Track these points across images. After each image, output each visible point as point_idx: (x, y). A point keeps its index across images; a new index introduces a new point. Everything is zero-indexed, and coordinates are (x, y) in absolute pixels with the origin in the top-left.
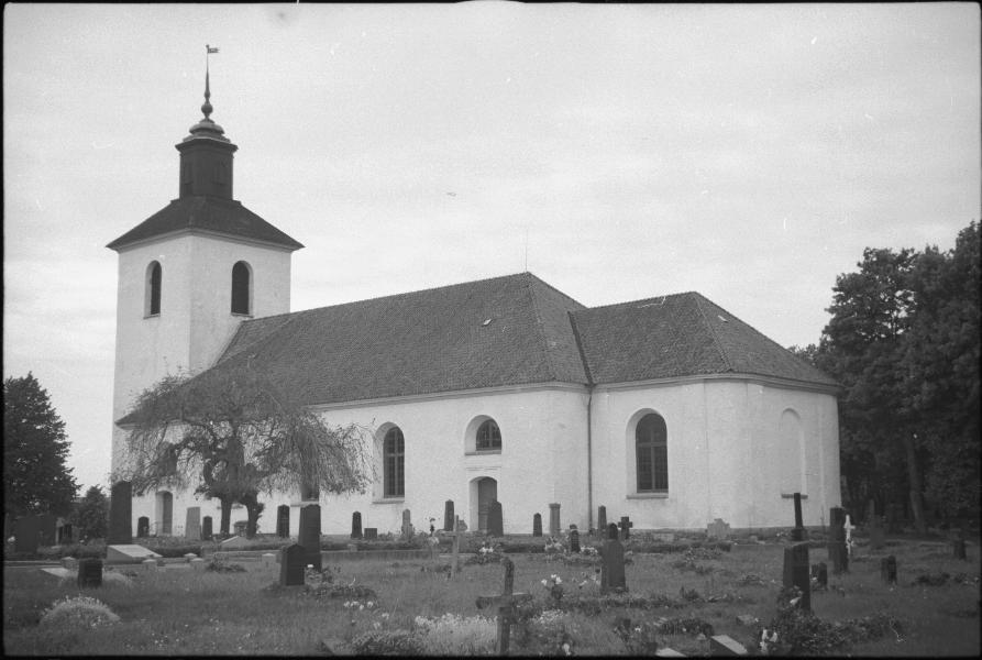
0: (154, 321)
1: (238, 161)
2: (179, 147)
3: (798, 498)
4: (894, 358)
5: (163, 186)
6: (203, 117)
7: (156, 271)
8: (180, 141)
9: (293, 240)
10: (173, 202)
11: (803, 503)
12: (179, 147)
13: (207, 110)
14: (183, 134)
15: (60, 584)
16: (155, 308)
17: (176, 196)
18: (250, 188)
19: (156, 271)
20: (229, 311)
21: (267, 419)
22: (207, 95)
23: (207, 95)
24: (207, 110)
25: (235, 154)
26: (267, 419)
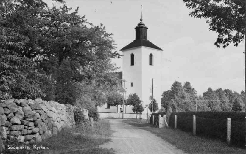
0: (133, 66)
1: (148, 31)
2: (135, 28)
3: (153, 79)
4: (65, 147)
5: (132, 38)
6: (140, 22)
7: (132, 56)
8: (135, 27)
9: (151, 43)
10: (134, 41)
11: (153, 80)
12: (135, 28)
13: (141, 20)
14: (136, 26)
15: (198, 117)
16: (132, 63)
17: (135, 39)
18: (150, 38)
19: (132, 56)
20: (149, 64)
21: (76, 69)
22: (141, 17)
23: (141, 17)
24: (141, 20)
25: (148, 30)
26: (76, 69)
